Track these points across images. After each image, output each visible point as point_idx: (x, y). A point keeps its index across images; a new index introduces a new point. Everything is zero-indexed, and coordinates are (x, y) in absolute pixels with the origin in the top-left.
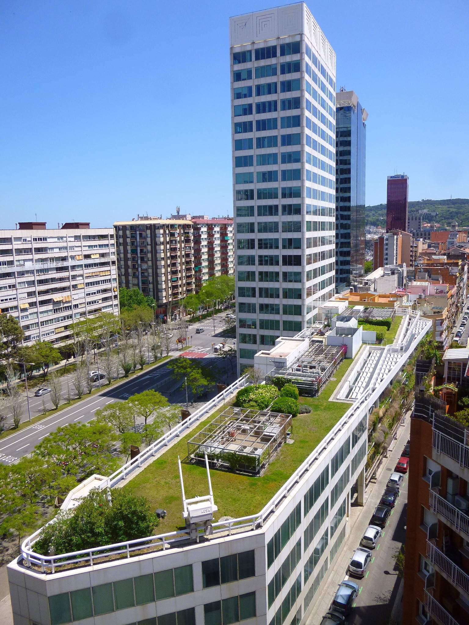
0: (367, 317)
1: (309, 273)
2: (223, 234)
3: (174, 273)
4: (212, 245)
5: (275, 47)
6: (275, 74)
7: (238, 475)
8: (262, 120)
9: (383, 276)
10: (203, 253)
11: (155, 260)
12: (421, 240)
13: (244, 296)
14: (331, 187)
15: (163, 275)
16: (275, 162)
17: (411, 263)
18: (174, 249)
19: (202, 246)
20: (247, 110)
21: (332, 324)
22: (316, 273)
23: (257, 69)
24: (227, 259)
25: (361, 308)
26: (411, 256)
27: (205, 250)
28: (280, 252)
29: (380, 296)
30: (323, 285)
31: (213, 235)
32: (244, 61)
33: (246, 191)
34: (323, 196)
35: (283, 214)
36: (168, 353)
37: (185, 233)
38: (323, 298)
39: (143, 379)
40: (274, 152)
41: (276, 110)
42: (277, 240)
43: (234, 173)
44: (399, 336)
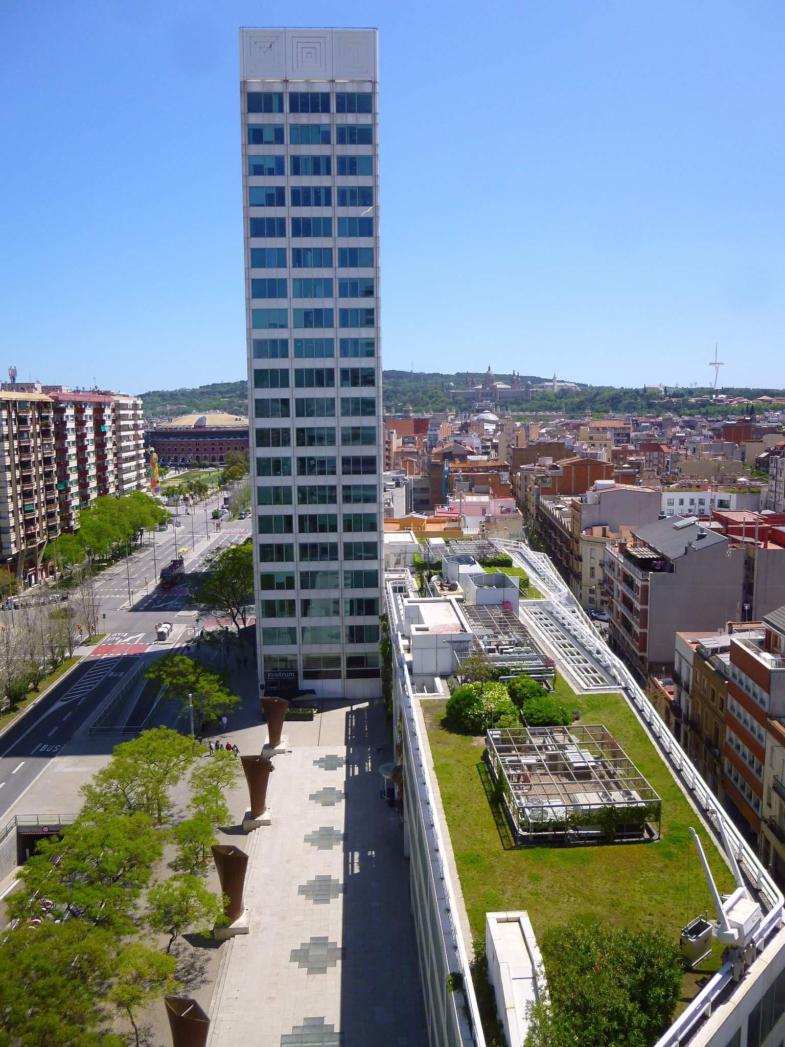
3: (27, 495)
5: (326, 96)
7: (627, 846)
16: (329, 294)
20: (275, 197)
23: (294, 128)
27: (72, 450)
39: (53, 709)
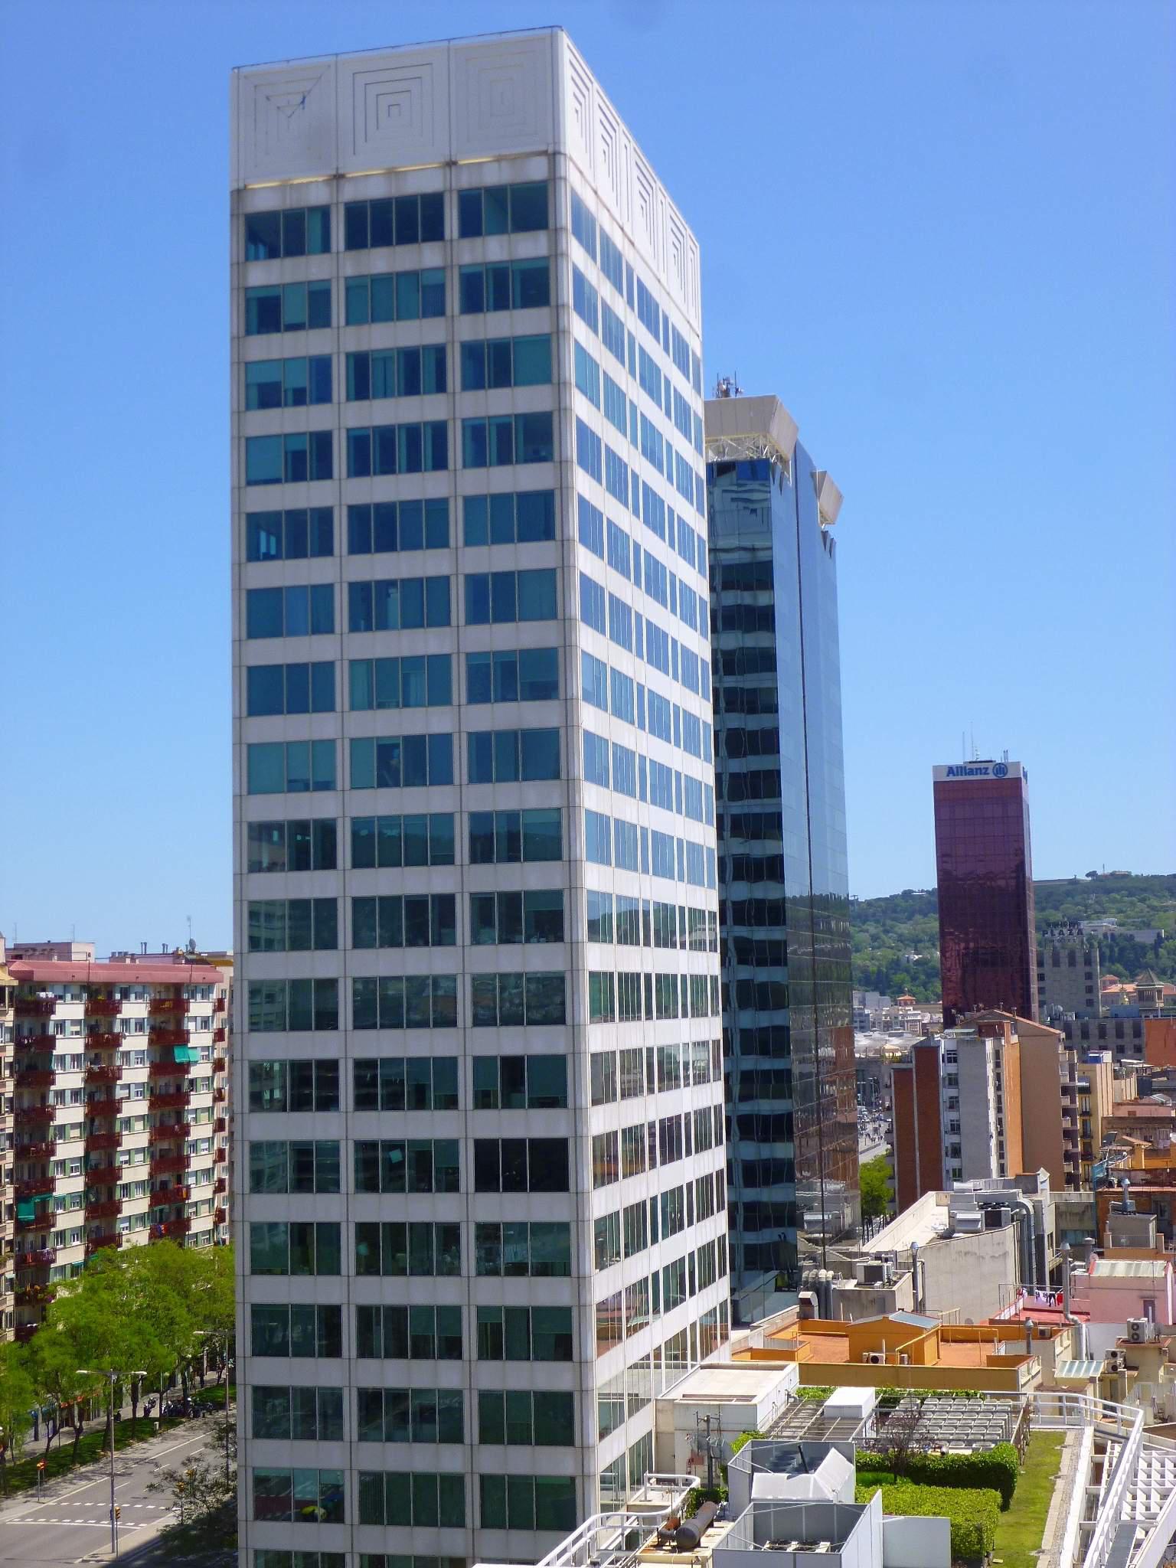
0: (902, 1446)
1: (606, 1225)
2: (167, 1035)
4: (110, 1090)
5: (434, 203)
9: (947, 1235)
10: (62, 1130)
12: (1107, 1056)
13: (280, 1351)
14: (694, 814)
16: (440, 696)
17: (1069, 1168)
19: (61, 1094)
20: (308, 459)
21: (735, 1487)
22: (638, 1227)
23: (354, 286)
24: (182, 1162)
25: (861, 1398)
26: (1068, 1134)
27: (70, 1114)
28: (465, 1126)
29: (947, 1336)
30: (676, 1283)
31: (116, 1041)
32: (296, 248)
33: (301, 827)
34: (661, 854)
35: (476, 940)
38: (677, 1353)
41: (440, 462)
42: (447, 1066)
43: (238, 742)
44: (1060, 1536)
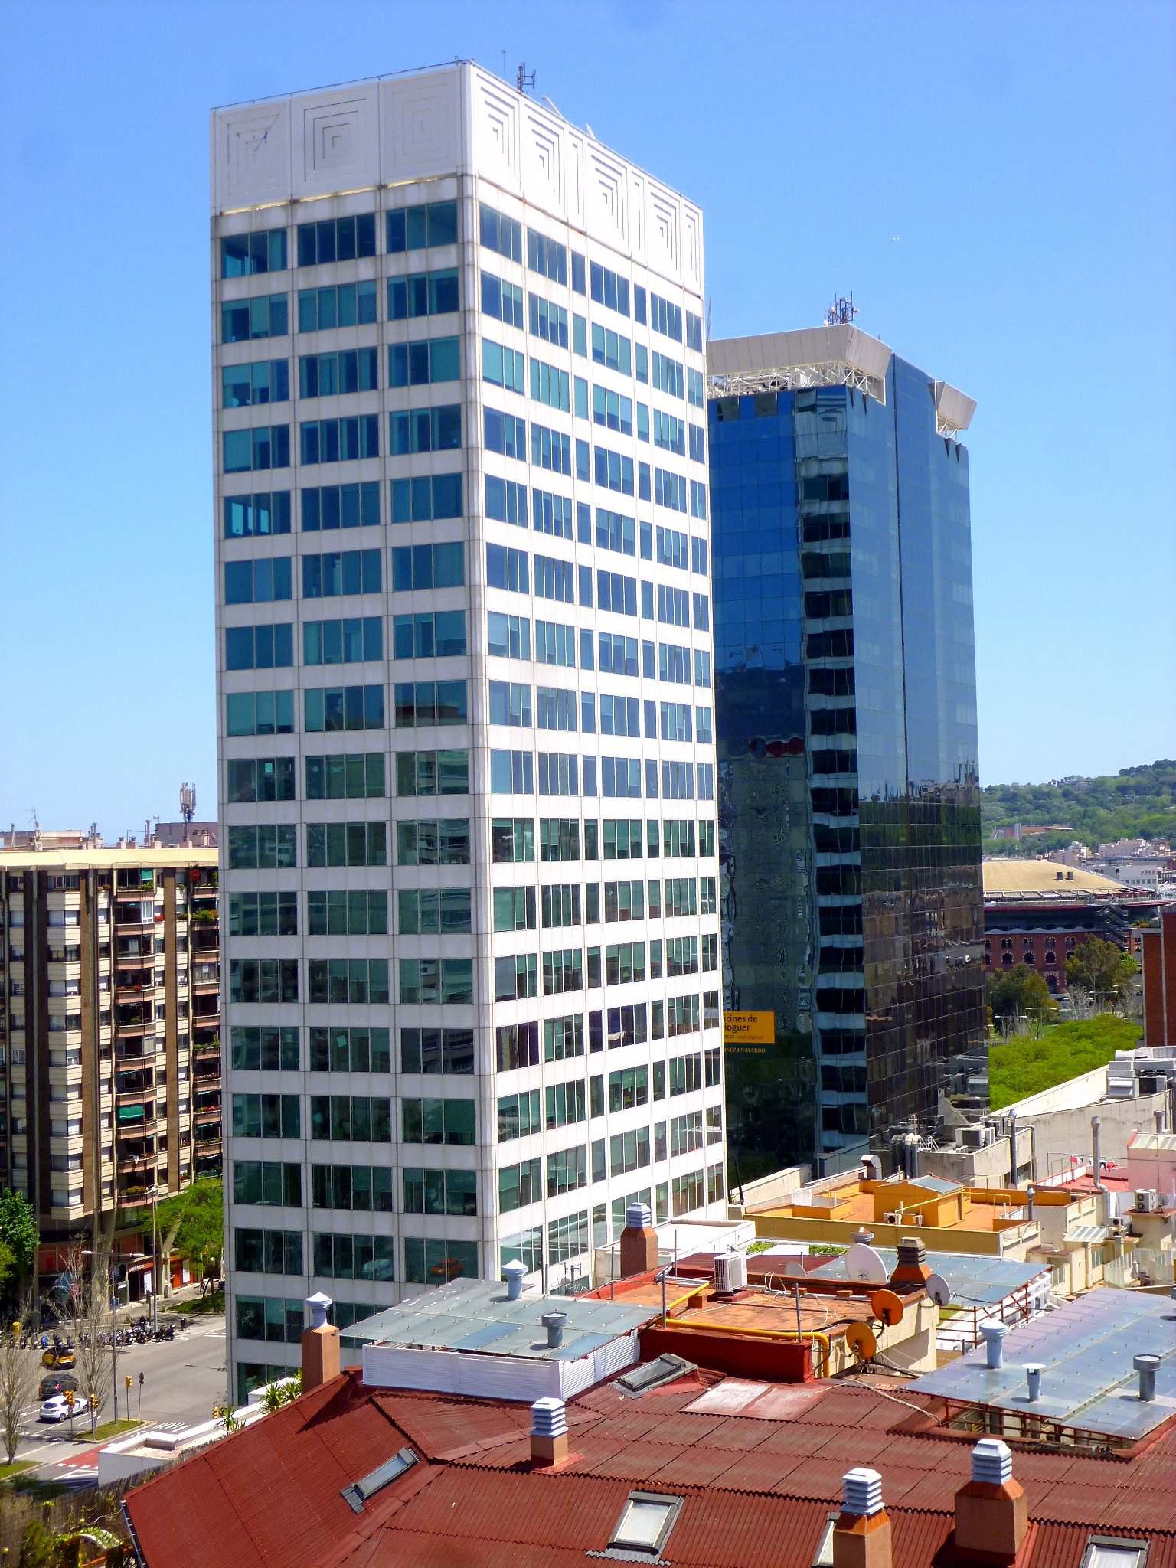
1: (509, 1107)
5: (366, 222)
6: (368, 316)
8: (325, 489)
11: (41, 1025)
15: (73, 1095)
16: (373, 653)
18: (142, 978)
20: (269, 450)
23: (306, 298)
35: (403, 861)
36: (11, 1454)
37: (196, 906)
40: (369, 613)
